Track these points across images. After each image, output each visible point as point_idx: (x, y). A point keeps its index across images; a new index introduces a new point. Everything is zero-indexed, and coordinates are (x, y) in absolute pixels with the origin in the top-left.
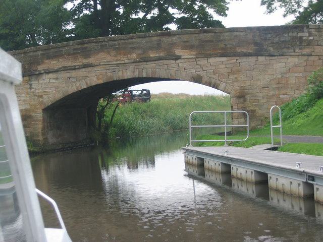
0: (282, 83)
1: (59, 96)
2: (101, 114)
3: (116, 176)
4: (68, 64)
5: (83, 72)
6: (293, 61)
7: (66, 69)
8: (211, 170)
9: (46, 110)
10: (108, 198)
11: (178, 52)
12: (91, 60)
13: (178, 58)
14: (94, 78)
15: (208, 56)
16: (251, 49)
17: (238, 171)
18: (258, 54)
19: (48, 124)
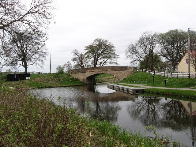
0: (123, 76)
1: (89, 76)
2: (95, 79)
3: (118, 105)
4: (91, 71)
5: (93, 72)
6: (125, 72)
7: (90, 72)
8: (125, 90)
9: (87, 78)
10: (96, 93)
11: (108, 70)
12: (94, 70)
13: (108, 71)
14: (94, 73)
15: (113, 71)
16: (119, 70)
17: (120, 88)
18: (120, 71)
19: (167, 93)
